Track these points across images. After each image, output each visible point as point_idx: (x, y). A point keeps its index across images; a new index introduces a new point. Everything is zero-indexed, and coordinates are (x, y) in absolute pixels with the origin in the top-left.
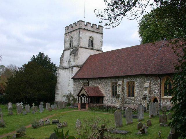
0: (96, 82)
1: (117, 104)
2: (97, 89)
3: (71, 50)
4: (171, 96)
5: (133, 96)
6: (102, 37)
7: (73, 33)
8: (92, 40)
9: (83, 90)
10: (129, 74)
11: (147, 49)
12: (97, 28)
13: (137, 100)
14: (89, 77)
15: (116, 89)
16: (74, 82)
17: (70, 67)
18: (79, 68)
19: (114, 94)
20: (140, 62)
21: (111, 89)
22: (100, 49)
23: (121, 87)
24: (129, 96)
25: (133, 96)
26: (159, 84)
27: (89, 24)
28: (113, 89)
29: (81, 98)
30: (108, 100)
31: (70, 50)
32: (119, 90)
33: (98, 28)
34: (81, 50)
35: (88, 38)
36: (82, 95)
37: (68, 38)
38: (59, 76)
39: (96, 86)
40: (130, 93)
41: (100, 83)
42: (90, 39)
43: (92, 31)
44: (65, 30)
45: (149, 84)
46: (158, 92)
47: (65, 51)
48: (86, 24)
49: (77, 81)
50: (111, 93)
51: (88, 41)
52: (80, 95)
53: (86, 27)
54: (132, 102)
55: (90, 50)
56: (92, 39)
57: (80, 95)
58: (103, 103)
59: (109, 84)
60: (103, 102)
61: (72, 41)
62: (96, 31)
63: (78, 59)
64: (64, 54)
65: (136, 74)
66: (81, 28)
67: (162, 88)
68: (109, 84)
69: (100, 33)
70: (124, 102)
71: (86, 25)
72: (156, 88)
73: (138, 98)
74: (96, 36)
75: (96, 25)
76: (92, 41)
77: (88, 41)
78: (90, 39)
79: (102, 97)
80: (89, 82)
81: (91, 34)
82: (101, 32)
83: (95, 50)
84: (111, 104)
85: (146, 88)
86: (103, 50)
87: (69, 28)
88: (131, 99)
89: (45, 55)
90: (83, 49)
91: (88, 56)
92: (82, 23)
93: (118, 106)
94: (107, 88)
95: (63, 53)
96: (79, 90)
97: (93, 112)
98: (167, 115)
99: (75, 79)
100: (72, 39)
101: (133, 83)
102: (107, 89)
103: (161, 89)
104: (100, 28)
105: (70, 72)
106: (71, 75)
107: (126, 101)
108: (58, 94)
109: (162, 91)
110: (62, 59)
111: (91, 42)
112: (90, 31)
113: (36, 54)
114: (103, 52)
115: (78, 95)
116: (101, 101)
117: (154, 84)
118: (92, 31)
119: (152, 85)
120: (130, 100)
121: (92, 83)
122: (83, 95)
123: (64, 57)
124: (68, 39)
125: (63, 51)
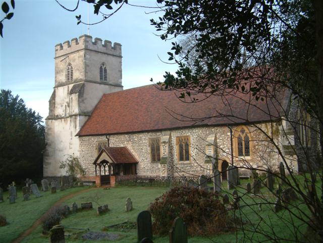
1: (161, 171)
2: (121, 152)
3: (71, 86)
4: (249, 156)
5: (188, 159)
6: (121, 62)
7: (72, 56)
9: (104, 154)
16: (80, 140)
17: (71, 116)
18: (87, 117)
19: (156, 157)
20: (196, 106)
21: (149, 149)
24: (181, 159)
25: (188, 159)
26: (229, 139)
27: (99, 42)
28: (152, 150)
30: (146, 168)
31: (67, 86)
32: (164, 151)
36: (101, 162)
38: (50, 132)
39: (122, 146)
40: (183, 155)
41: (130, 140)
42: (101, 68)
44: (57, 50)
45: (213, 138)
49: (86, 138)
50: (149, 157)
52: (99, 162)
53: (95, 46)
55: (102, 86)
56: (105, 66)
57: (99, 162)
58: (136, 174)
59: (146, 141)
60: (136, 172)
61: (70, 70)
63: (85, 101)
67: (234, 143)
68: (146, 141)
69: (118, 56)
72: (225, 146)
74: (112, 60)
76: (105, 71)
77: (98, 71)
79: (135, 164)
80: (108, 140)
81: (104, 58)
82: (117, 54)
84: (151, 175)
87: (64, 48)
88: (184, 164)
89: (14, 94)
90: (91, 83)
91: (100, 95)
93: (164, 177)
94: (142, 149)
96: (96, 156)
99: (80, 135)
100: (70, 67)
103: (234, 147)
104: (117, 46)
106: (73, 129)
109: (234, 150)
110: (53, 101)
112: (101, 52)
114: (124, 89)
115: (95, 163)
116: (134, 170)
117: (221, 138)
119: (218, 140)
120: (182, 166)
121: (115, 141)
122: (104, 162)
124: (63, 66)
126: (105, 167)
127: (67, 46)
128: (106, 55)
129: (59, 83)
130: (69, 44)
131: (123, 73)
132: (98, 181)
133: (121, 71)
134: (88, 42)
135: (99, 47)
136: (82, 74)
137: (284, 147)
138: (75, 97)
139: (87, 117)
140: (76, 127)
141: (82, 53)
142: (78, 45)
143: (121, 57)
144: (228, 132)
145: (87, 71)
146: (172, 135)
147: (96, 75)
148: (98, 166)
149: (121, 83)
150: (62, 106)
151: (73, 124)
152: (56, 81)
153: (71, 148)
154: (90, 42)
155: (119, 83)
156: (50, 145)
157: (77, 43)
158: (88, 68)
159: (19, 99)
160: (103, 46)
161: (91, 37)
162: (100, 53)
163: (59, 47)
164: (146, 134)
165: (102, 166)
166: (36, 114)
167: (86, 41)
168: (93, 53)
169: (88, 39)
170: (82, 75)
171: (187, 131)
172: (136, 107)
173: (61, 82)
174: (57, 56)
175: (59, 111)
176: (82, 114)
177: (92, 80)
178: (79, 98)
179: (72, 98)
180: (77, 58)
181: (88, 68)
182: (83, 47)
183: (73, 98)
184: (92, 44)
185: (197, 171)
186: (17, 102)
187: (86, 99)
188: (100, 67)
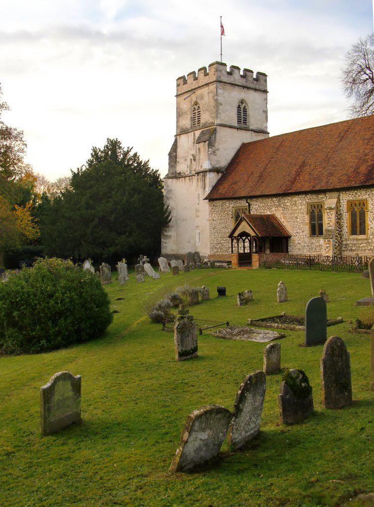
0: (269, 204)
1: (324, 249)
3: (198, 133)
5: (363, 232)
6: (266, 99)
7: (199, 92)
8: (245, 107)
12: (254, 79)
15: (320, 218)
17: (198, 173)
19: (316, 229)
21: (307, 218)
22: (263, 128)
23: (333, 212)
24: (353, 232)
25: (363, 232)
28: (312, 218)
31: (193, 133)
32: (329, 221)
33: (257, 80)
34: (222, 133)
41: (280, 206)
42: (239, 107)
43: (244, 87)
44: (178, 85)
48: (228, 70)
49: (219, 203)
51: (236, 111)
52: (236, 234)
53: (230, 76)
54: (362, 245)
56: (244, 105)
57: (236, 234)
58: (287, 252)
60: (287, 249)
61: (196, 111)
63: (217, 153)
64: (178, 144)
66: (219, 79)
70: (340, 246)
71: (230, 74)
74: (251, 97)
75: (252, 72)
76: (245, 110)
77: (235, 111)
78: (239, 106)
80: (249, 205)
82: (262, 88)
86: (268, 131)
89: (125, 146)
91: (237, 145)
92: (221, 67)
95: (176, 141)
97: (29, 355)
98: (250, 501)
99: (211, 198)
101: (363, 204)
102: (298, 220)
106: (200, 191)
107: (347, 245)
110: (174, 154)
111: (242, 112)
113: (101, 145)
114: (271, 135)
120: (355, 242)
122: (244, 234)
123: (178, 150)
124: (186, 106)
125: (175, 136)
132: (235, 260)
133: (266, 112)
135: (236, 78)
140: (205, 188)
148: (235, 241)
149: (267, 128)
150: (186, 160)
151: (200, 184)
154: (223, 72)
157: (206, 74)
164: (304, 196)
168: (228, 87)
171: (363, 192)
174: (179, 93)
183: (202, 149)
187: (218, 150)
188: (237, 106)
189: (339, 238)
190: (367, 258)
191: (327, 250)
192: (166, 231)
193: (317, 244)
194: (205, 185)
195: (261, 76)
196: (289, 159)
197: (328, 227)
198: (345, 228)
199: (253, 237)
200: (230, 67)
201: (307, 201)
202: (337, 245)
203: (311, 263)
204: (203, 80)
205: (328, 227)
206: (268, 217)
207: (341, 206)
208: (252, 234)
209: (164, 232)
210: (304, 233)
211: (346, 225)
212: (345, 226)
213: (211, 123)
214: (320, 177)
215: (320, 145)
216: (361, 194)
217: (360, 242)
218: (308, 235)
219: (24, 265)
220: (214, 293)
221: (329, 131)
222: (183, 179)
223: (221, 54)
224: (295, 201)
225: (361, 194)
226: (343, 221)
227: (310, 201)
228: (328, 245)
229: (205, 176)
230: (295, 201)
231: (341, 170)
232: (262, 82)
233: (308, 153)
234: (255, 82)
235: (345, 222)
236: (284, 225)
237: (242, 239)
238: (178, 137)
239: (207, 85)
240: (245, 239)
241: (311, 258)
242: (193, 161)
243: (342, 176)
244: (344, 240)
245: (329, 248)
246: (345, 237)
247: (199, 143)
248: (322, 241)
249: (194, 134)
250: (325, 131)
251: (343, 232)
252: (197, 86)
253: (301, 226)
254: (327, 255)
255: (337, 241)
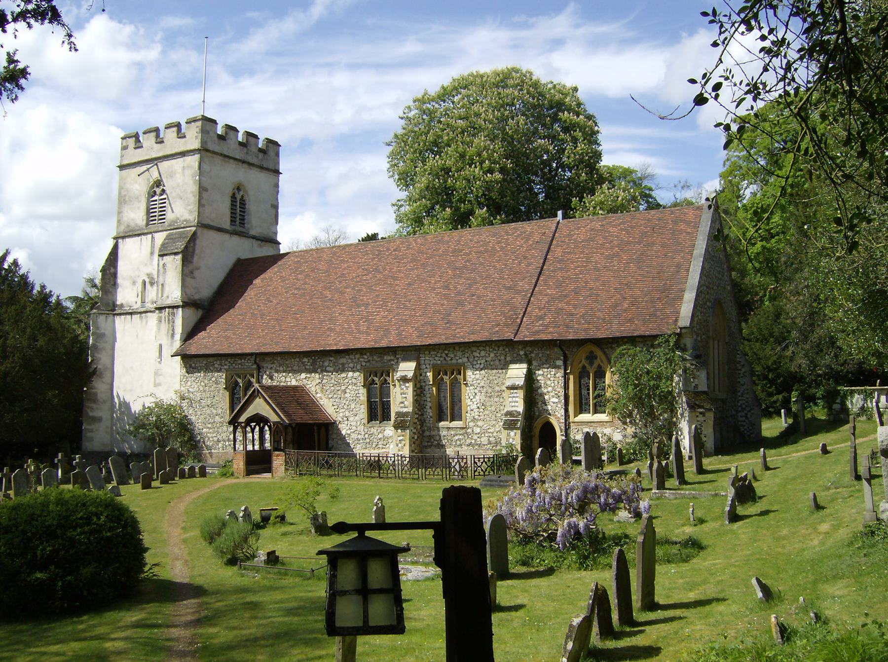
3: (160, 238)
7: (164, 165)
10: (443, 340)
11: (493, 248)
13: (478, 430)
14: (263, 350)
17: (160, 309)
29: (245, 433)
31: (150, 236)
35: (229, 191)
36: (249, 421)
37: (137, 186)
42: (233, 197)
43: (244, 162)
44: (124, 148)
46: (556, 400)
47: (123, 237)
48: (220, 131)
52: (243, 419)
53: (222, 142)
54: (456, 438)
55: (235, 239)
56: (241, 193)
57: (243, 419)
60: (327, 443)
62: (254, 161)
63: (197, 274)
65: (473, 338)
71: (221, 138)
73: (480, 423)
74: (254, 179)
75: (256, 137)
76: (243, 203)
78: (234, 194)
81: (241, 174)
82: (271, 166)
83: (254, 237)
85: (513, 388)
91: (229, 262)
95: (115, 248)
105: (159, 328)
106: (165, 341)
108: (99, 420)
110: (112, 270)
112: (235, 159)
118: (244, 162)
122: (259, 419)
125: (116, 238)
126: (253, 431)
127: (154, 140)
128: (245, 165)
129: (128, 226)
130: (158, 136)
131: (279, 211)
132: (239, 464)
133: (275, 207)
134: (208, 132)
135: (230, 148)
136: (190, 207)
137: (460, 374)
138: (174, 263)
139: (200, 313)
140: (173, 335)
141: (194, 160)
142: (139, 150)
143: (277, 172)
144: (559, 359)
145: (203, 202)
146: (422, 362)
147: (222, 213)
148: (239, 430)
149: (276, 233)
150: (134, 283)
151: (164, 327)
152: (119, 221)
153: (159, 384)
154: (212, 134)
155: (271, 234)
156: (101, 376)
157: (181, 135)
158: (205, 194)
159: (10, 259)
160: (241, 144)
161: (214, 122)
162: (231, 161)
163: (131, 142)
164: (358, 356)
165: (248, 429)
166: (53, 300)
167: (204, 131)
168: (218, 160)
169: (209, 126)
170: (191, 212)
171: (459, 354)
172: (328, 293)
173: (132, 224)
174: (126, 162)
175: (126, 295)
176: (187, 304)
177: (212, 224)
178: (183, 265)
179: (164, 265)
180: (180, 170)
181: (205, 194)
182: (196, 144)
183: (169, 266)
184: (216, 138)
185: (479, 445)
186: (6, 266)
187: (198, 268)
188: (231, 195)
189: (419, 427)
190: (474, 458)
191: (400, 445)
192: (92, 409)
193: (380, 436)
194: (173, 330)
195: (270, 145)
196: (328, 293)
197: (402, 407)
198: (429, 411)
199: (274, 423)
200: (223, 127)
201: (364, 364)
202: (416, 437)
203: (376, 466)
204: (173, 143)
205: (402, 407)
206: (295, 388)
207: (421, 375)
208: (273, 418)
209: (89, 411)
210: (357, 418)
211: (429, 404)
212: (428, 407)
213: (185, 221)
214: (386, 325)
215: (381, 273)
216: (455, 356)
217: (453, 433)
218: (365, 421)
219: (132, 482)
220: (740, 510)
221: (395, 250)
222: (129, 317)
223: (204, 101)
224: (343, 364)
225: (455, 356)
226: (424, 398)
227: (368, 364)
228: (401, 438)
229: (174, 314)
230: (343, 364)
231: (420, 316)
232: (271, 153)
233: (361, 285)
234: (261, 155)
235: (429, 400)
236: (322, 403)
237: (251, 426)
238: (120, 241)
239: (183, 154)
240: (255, 426)
241: (372, 458)
242: (148, 286)
243: (423, 325)
244: (426, 428)
245: (403, 442)
246: (428, 425)
247: (166, 255)
248: (389, 430)
249: (153, 238)
250: (388, 250)
251: (425, 416)
252: (160, 154)
253: (353, 406)
254: (400, 453)
255: (415, 431)
